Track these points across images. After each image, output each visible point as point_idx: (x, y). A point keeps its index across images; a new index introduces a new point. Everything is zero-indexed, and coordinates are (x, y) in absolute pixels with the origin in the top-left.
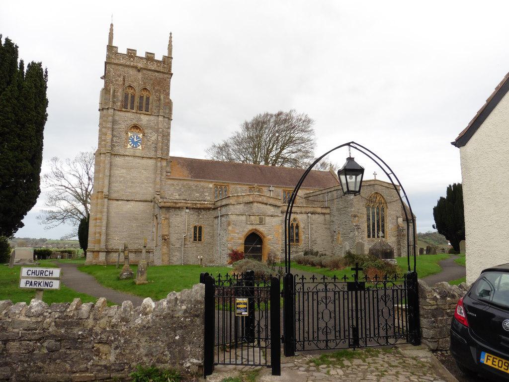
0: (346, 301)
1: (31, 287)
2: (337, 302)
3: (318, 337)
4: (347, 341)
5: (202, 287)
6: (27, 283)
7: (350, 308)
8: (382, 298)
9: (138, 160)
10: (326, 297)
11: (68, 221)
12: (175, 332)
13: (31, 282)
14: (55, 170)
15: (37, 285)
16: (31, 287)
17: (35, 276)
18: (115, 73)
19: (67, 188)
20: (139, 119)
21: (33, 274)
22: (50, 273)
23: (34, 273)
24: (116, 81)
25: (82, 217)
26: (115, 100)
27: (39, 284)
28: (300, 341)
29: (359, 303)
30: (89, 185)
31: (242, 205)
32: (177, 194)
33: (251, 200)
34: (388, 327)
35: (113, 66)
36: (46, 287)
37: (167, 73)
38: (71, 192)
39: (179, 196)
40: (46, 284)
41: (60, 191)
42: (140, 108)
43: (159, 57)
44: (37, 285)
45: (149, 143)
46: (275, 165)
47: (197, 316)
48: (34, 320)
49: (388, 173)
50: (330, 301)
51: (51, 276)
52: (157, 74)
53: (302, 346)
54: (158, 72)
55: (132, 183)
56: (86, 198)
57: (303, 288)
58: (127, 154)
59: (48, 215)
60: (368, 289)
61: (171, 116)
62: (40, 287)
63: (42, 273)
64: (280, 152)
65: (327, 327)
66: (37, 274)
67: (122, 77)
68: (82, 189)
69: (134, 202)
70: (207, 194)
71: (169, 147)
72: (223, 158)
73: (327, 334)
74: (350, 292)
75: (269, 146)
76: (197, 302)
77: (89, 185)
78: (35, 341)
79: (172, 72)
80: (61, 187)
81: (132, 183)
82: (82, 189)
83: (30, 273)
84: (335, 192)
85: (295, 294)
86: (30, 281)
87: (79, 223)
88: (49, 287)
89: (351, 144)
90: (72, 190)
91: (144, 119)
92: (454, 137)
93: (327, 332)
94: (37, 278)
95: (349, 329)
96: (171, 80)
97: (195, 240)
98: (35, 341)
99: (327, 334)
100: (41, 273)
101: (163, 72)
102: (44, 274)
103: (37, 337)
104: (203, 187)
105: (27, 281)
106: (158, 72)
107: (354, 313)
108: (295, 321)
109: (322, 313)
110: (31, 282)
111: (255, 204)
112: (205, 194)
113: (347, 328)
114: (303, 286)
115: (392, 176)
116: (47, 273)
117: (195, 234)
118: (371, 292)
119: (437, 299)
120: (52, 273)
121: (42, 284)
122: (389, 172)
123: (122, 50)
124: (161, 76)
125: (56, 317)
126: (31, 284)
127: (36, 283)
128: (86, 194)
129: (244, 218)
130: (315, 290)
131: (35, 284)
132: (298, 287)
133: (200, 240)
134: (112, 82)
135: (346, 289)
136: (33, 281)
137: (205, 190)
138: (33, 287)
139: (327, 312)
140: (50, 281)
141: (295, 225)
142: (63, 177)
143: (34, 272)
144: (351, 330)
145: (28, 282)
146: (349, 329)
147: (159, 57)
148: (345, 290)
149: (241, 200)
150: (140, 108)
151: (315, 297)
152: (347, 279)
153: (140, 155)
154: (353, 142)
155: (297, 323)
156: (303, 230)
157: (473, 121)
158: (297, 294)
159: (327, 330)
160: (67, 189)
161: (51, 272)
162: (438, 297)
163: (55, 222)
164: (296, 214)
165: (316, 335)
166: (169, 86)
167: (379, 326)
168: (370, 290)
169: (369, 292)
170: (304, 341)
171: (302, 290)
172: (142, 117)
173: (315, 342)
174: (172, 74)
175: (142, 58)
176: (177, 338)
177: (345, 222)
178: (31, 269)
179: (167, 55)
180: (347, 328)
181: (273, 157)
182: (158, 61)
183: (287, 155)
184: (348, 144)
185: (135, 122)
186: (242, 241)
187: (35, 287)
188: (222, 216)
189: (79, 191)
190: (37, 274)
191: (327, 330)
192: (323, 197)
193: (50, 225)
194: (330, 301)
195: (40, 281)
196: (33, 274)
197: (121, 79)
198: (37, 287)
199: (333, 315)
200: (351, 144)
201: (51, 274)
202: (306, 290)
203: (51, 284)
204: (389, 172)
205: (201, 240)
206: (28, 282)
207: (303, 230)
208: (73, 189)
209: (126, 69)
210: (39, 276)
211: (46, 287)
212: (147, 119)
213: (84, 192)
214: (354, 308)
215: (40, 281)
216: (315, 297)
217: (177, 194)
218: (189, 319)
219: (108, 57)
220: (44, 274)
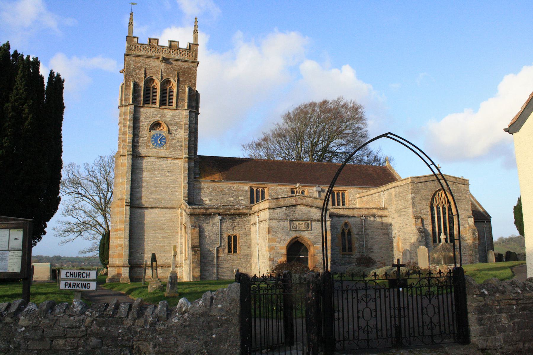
0: (387, 299)
1: (70, 288)
2: (378, 300)
3: (358, 336)
4: (390, 340)
5: (238, 285)
6: (66, 285)
7: (392, 306)
8: (426, 296)
9: (162, 162)
10: (366, 295)
11: (86, 234)
12: (211, 330)
13: (70, 283)
14: (71, 176)
15: (76, 286)
16: (70, 288)
17: (74, 278)
18: (135, 66)
19: (84, 196)
20: (163, 116)
21: (71, 276)
22: (87, 275)
23: (72, 275)
24: (137, 74)
25: (102, 231)
26: (136, 95)
27: (78, 286)
28: (339, 341)
29: (401, 300)
30: (108, 191)
31: (284, 209)
32: (207, 199)
33: (294, 202)
34: (433, 325)
35: (133, 58)
36: (84, 289)
37: (192, 62)
38: (88, 200)
39: (210, 201)
40: (84, 286)
41: (76, 199)
42: (163, 103)
43: (183, 45)
44: (76, 286)
45: (174, 142)
46: (321, 161)
47: (233, 315)
48: (77, 318)
49: (429, 164)
50: (371, 299)
51: (88, 278)
52: (181, 63)
53: (342, 345)
54: (182, 61)
55: (156, 187)
56: (105, 208)
57: (342, 286)
58: (150, 154)
59: (65, 227)
60: (411, 286)
61: (198, 110)
62: (78, 288)
63: (80, 275)
64: (328, 145)
65: (368, 325)
66: (75, 276)
67: (143, 70)
68: (100, 198)
69: (159, 209)
70: (242, 198)
71: (197, 146)
72: (262, 154)
73: (368, 334)
74: (391, 290)
75: (314, 138)
76: (232, 300)
77: (108, 191)
78: (78, 339)
79: (198, 60)
80: (76, 196)
81: (156, 187)
82: (100, 198)
83: (68, 275)
84: (393, 189)
85: (334, 292)
86: (69, 282)
87: (100, 237)
88: (86, 289)
89: (389, 135)
90: (89, 199)
91: (168, 114)
92: (506, 124)
93: (368, 331)
94: (75, 280)
95: (391, 328)
96: (198, 69)
97: (230, 251)
98: (78, 339)
99: (368, 334)
100: (79, 275)
101: (188, 61)
102: (81, 276)
103: (79, 334)
104: (238, 190)
105: (66, 283)
106: (182, 61)
107: (397, 312)
108: (334, 320)
109: (363, 312)
110: (70, 283)
111: (299, 207)
112: (240, 198)
113: (389, 327)
114: (342, 283)
115: (433, 167)
116: (85, 275)
117: (229, 244)
118: (414, 289)
119: (485, 295)
120: (89, 275)
121: (80, 285)
122: (430, 163)
123: (144, 40)
124: (186, 65)
125: (97, 316)
126: (70, 286)
127: (74, 284)
128: (105, 203)
129: (287, 223)
130: (354, 288)
131: (73, 285)
132: (337, 285)
133: (235, 251)
134: (132, 76)
135: (388, 287)
136: (72, 282)
137: (240, 193)
138: (72, 289)
139: (367, 311)
140: (87, 283)
141: (346, 231)
142: (80, 184)
143: (72, 273)
144: (394, 329)
145: (67, 284)
146: (391, 328)
147: (183, 45)
148: (386, 287)
149: (282, 202)
150: (163, 103)
151: (355, 295)
152: (388, 276)
153: (164, 155)
154: (390, 133)
155: (336, 323)
156: (357, 236)
157: (525, 106)
158: (336, 292)
159: (368, 329)
160: (84, 198)
161: (88, 274)
162: (486, 292)
163: (72, 236)
164: (347, 218)
165: (356, 334)
166: (195, 76)
167: (423, 325)
168: (413, 287)
169: (412, 289)
170: (344, 340)
171: (341, 288)
172: (166, 111)
173: (356, 341)
174: (198, 63)
175: (164, 47)
176: (214, 336)
177: (406, 225)
178: (69, 271)
179: (192, 42)
180: (389, 327)
181: (319, 151)
182: (183, 50)
183: (335, 148)
184: (385, 135)
185: (158, 118)
186: (284, 251)
187: (74, 288)
188: (259, 222)
189: (97, 199)
190: (75, 276)
191: (368, 329)
192: (379, 196)
193: (67, 238)
194: (371, 299)
195: (78, 282)
196: (71, 276)
197: (143, 71)
198: (76, 289)
199: (374, 314)
200: (389, 135)
201: (88, 276)
202: (345, 288)
203: (88, 285)
204: (430, 163)
205: (237, 252)
206: (67, 284)
207: (357, 236)
208: (91, 198)
209: (148, 60)
210: (77, 278)
211: (84, 289)
212: (172, 114)
213: (103, 201)
214: (396, 306)
215: (78, 282)
216: (355, 295)
217: (207, 199)
218: (226, 318)
219: (129, 49)
220: (81, 276)
